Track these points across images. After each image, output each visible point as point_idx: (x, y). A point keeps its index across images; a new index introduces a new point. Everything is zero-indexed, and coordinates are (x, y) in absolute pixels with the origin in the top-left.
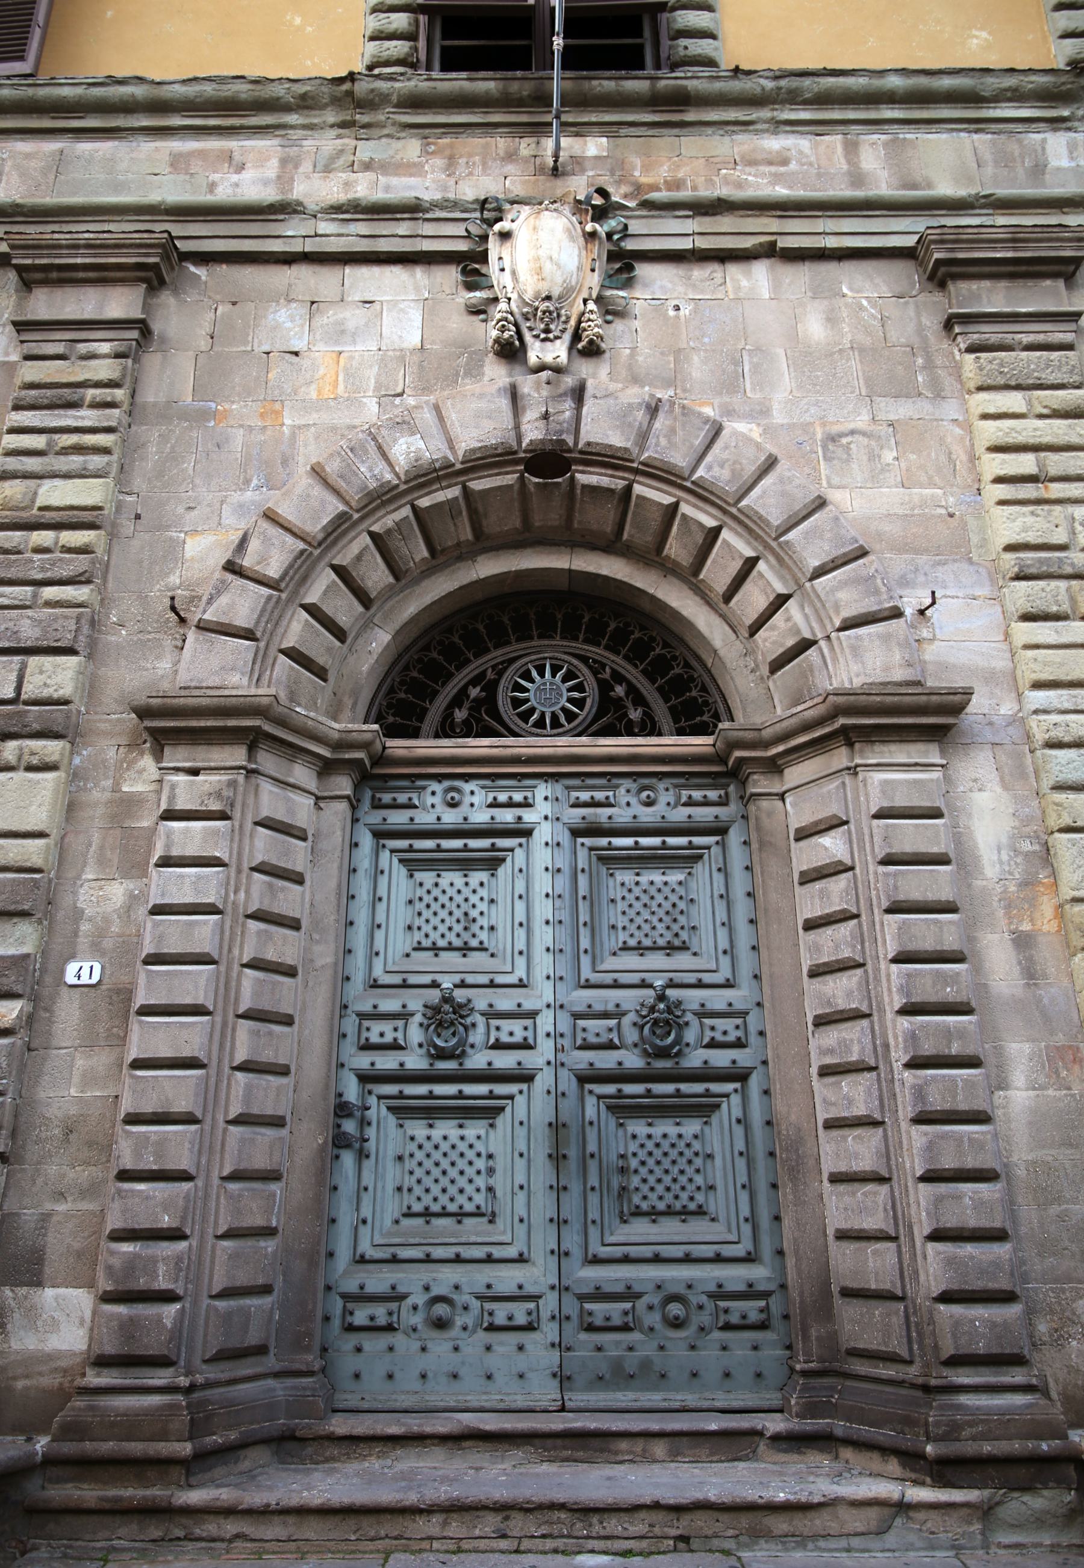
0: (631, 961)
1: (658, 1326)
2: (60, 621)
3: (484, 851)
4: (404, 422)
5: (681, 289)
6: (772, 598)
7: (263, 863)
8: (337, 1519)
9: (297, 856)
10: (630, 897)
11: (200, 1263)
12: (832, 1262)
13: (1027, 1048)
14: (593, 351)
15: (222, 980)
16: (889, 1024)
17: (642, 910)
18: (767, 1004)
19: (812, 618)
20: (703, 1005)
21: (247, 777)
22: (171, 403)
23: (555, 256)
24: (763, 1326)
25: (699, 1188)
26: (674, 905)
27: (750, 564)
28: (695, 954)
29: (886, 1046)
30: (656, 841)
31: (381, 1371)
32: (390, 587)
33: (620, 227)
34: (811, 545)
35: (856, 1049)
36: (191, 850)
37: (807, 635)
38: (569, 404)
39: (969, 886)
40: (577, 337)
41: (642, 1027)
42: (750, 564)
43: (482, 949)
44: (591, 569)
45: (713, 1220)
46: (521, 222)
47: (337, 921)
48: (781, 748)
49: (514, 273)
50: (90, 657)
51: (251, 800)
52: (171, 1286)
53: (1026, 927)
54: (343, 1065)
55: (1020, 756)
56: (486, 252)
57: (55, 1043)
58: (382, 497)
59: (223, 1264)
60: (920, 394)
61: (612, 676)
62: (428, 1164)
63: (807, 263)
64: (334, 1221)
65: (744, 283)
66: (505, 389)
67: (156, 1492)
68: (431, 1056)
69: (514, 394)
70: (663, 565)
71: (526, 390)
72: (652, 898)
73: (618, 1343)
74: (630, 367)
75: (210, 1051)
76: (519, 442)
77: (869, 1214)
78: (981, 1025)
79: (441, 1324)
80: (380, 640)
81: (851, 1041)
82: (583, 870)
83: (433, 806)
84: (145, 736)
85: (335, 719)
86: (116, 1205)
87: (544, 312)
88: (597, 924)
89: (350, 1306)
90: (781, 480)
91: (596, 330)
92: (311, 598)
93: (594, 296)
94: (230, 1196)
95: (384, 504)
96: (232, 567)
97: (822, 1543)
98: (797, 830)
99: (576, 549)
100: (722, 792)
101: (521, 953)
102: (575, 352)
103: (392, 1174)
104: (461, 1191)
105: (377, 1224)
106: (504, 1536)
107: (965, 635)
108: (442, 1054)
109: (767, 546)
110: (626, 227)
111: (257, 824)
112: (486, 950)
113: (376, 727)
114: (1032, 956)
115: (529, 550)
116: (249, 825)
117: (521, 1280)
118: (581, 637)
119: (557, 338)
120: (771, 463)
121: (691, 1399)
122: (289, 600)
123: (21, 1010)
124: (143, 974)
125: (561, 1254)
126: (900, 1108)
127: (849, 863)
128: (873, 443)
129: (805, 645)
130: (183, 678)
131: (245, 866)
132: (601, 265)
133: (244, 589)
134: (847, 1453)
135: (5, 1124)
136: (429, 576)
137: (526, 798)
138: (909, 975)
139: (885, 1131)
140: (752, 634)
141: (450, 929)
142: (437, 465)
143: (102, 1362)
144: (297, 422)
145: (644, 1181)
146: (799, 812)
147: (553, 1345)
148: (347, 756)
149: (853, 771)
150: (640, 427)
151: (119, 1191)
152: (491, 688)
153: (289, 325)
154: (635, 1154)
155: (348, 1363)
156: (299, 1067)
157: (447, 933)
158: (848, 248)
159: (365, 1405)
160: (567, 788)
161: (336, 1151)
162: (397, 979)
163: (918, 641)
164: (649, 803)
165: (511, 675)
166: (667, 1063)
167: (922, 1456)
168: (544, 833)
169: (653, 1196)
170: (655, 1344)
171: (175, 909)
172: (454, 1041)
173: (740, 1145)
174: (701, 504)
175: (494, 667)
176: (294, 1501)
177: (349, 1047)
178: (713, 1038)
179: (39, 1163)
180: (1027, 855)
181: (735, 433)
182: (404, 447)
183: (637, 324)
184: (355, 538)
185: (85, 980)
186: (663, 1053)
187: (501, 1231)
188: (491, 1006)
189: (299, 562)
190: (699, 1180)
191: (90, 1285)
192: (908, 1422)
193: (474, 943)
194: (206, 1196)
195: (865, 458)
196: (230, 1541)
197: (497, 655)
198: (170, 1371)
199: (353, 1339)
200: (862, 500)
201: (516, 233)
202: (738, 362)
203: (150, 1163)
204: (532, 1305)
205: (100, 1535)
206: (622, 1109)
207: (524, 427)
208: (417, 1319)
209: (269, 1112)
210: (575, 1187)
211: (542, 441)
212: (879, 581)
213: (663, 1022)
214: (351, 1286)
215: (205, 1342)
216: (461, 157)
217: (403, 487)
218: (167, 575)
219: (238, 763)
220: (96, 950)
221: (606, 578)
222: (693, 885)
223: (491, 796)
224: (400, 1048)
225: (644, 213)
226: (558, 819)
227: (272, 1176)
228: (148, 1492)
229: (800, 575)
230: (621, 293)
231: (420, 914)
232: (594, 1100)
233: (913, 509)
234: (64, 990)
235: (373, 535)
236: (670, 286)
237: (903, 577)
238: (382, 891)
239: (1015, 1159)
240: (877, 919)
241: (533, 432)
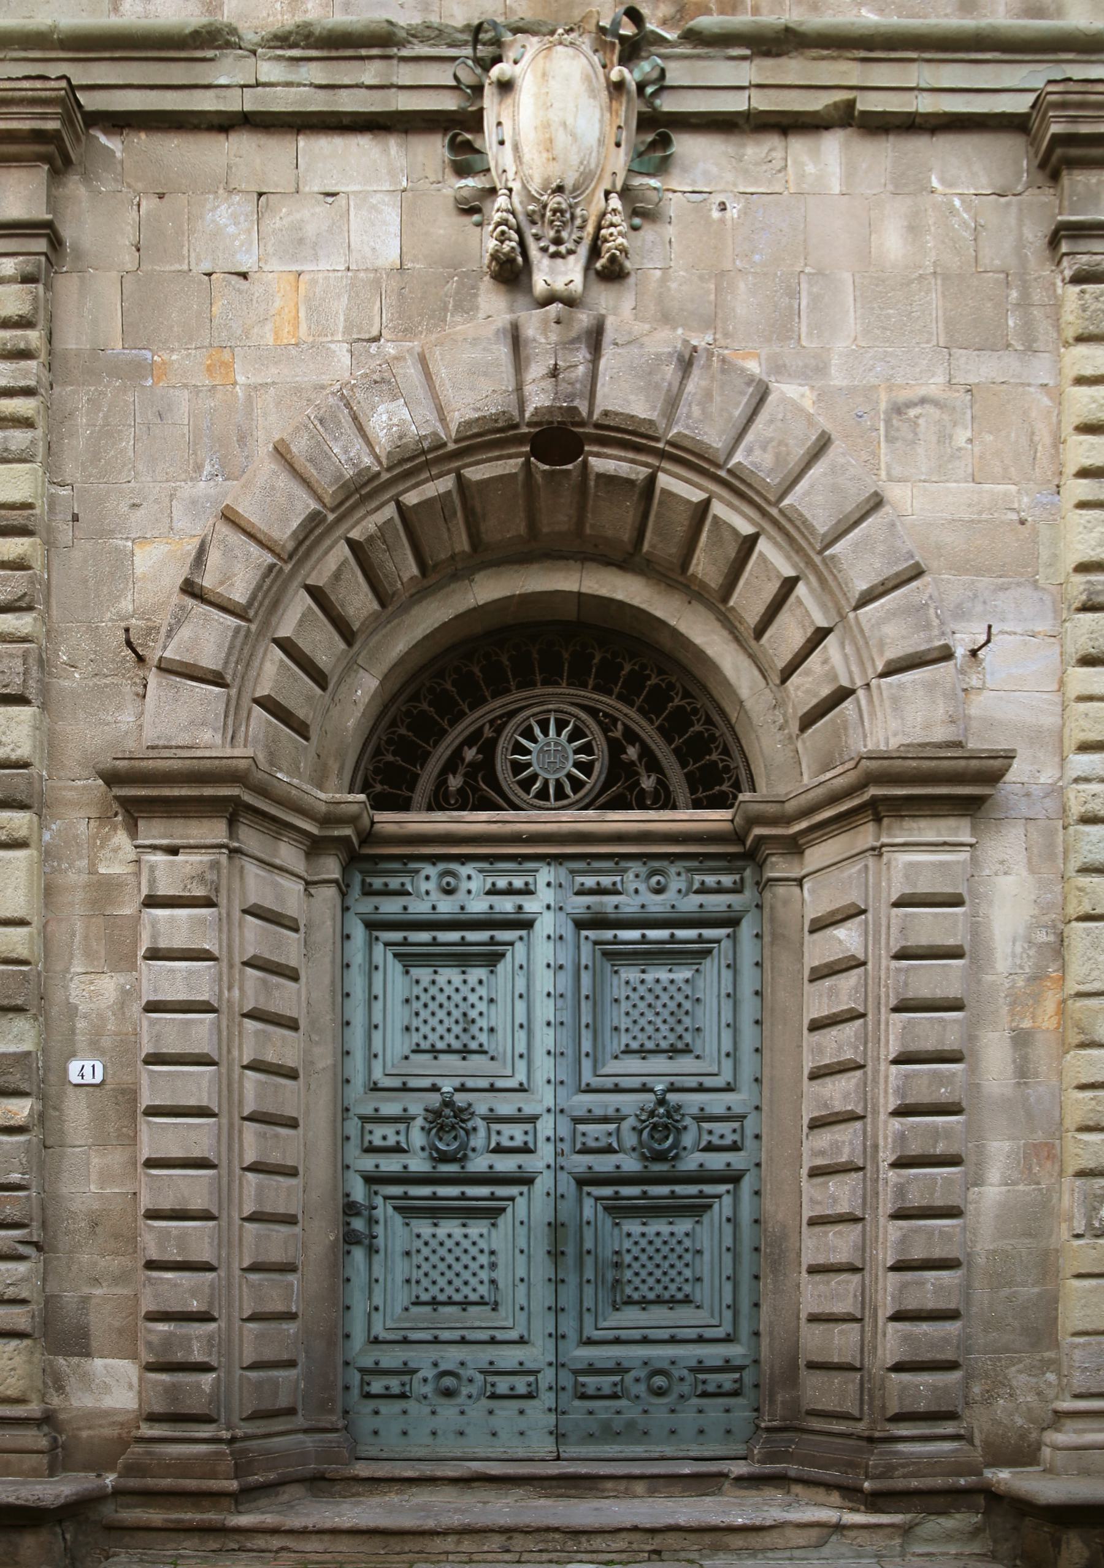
0: (633, 1064)
1: (643, 1395)
2: (6, 661)
3: (482, 943)
4: (383, 381)
5: (729, 176)
6: (810, 631)
7: (255, 957)
8: (364, 1538)
9: (289, 948)
10: (634, 996)
11: (229, 1341)
12: (801, 1341)
13: (1006, 1145)
15: (225, 1082)
16: (881, 1125)
17: (646, 1010)
18: (765, 1108)
19: (853, 660)
20: (702, 1109)
21: (230, 858)
22: (98, 351)
24: (735, 1394)
25: (687, 1280)
26: (679, 1005)
27: (789, 585)
28: (698, 1057)
29: (876, 1147)
30: (663, 934)
31: (396, 1427)
32: (375, 616)
33: (655, 74)
34: (860, 562)
35: (846, 1150)
36: (179, 941)
37: (845, 683)
38: (582, 354)
39: (979, 982)
40: (595, 252)
41: (641, 1132)
42: (789, 585)
43: (482, 1051)
44: (604, 592)
45: (698, 1307)
47: (333, 1020)
48: (804, 825)
49: (516, 148)
50: (43, 707)
51: (236, 885)
52: (206, 1359)
53: (1026, 1024)
54: (348, 1167)
55: (1050, 833)
57: (69, 1141)
58: (361, 491)
59: (251, 1342)
60: (1009, 345)
61: (624, 735)
62: (434, 1259)
63: (891, 138)
64: (348, 1308)
65: (810, 169)
67: (211, 1517)
68: (434, 1159)
69: (516, 338)
70: (687, 587)
72: (657, 997)
73: (607, 1408)
75: (219, 1152)
76: (522, 411)
77: (838, 1295)
78: (968, 1125)
79: (448, 1393)
80: (365, 688)
81: (843, 1142)
82: (586, 967)
83: (427, 893)
84: (116, 806)
85: (320, 787)
86: (148, 1290)
87: (554, 212)
88: (599, 1025)
89: (367, 1378)
90: (833, 470)
91: (620, 240)
92: (285, 631)
93: (619, 187)
94: (251, 1286)
95: (365, 499)
96: (191, 589)
97: (770, 1554)
98: (813, 921)
99: (588, 564)
100: (737, 877)
101: (521, 1056)
102: (592, 273)
103: (401, 1268)
104: (466, 1283)
105: (388, 1310)
106: (508, 1551)
107: (1013, 686)
108: (444, 1158)
109: (810, 563)
110: (663, 72)
111: (245, 911)
112: (486, 1052)
113: (362, 797)
114: (1027, 1054)
115: (535, 567)
116: (237, 914)
117: (522, 1359)
118: (591, 682)
119: (571, 252)
120: (823, 445)
121: (669, 1451)
122: (260, 633)
123: (31, 1109)
124: (146, 1073)
125: (558, 1337)
126: (881, 1205)
127: (862, 957)
128: (945, 417)
129: (842, 694)
130: (150, 735)
131: (237, 960)
133: (207, 619)
134: (797, 1489)
135: (35, 1216)
136: (420, 601)
137: (527, 884)
138: (907, 1076)
139: (864, 1227)
140: (784, 681)
141: (449, 1030)
142: (426, 445)
143: (153, 1418)
144: (252, 381)
145: (637, 1274)
146: (816, 901)
147: (550, 1410)
148: (336, 833)
149: (877, 851)
150: (669, 390)
151: (149, 1279)
152: (489, 749)
153: (232, 229)
154: (628, 1251)
155: (366, 1423)
156: (307, 1169)
157: (446, 1035)
158: (946, 114)
159: (385, 1455)
160: (572, 872)
161: (347, 1247)
162: (396, 1083)
163: (965, 690)
164: (659, 890)
165: (511, 733)
166: (662, 1166)
167: (860, 1490)
168: (546, 924)
169: (644, 1288)
170: (640, 1409)
171: (169, 1007)
172: (455, 1146)
173: (728, 1241)
174: (736, 502)
175: (492, 722)
176: (328, 1525)
177: (353, 1151)
178: (710, 1142)
179: (71, 1252)
180: (1040, 946)
181: (784, 399)
182: (384, 417)
183: (670, 231)
184: (331, 548)
185: (88, 1079)
186: (660, 1157)
187: (503, 1317)
188: (491, 1110)
189: (268, 581)
190: (688, 1273)
191: (134, 1357)
192: (852, 1465)
193: (473, 1045)
194: (229, 1285)
195: (934, 439)
196: (277, 1552)
197: (496, 706)
198: (213, 1427)
199: (372, 1404)
200: (927, 500)
201: (519, 82)
202: (794, 294)
203: (174, 1255)
204: (532, 1379)
205: (168, 1546)
206: (618, 1210)
207: (528, 389)
208: (427, 1389)
209: (282, 1210)
210: (572, 1279)
211: (550, 409)
212: (932, 611)
213: (662, 1126)
214: (368, 1362)
215: (241, 1404)
217: (386, 476)
218: (117, 599)
219: (218, 841)
220: (96, 1049)
221: (621, 604)
222: (700, 983)
223: (490, 880)
224: (404, 1151)
226: (561, 908)
227: (289, 1268)
228: (205, 1516)
229: (843, 602)
230: (653, 182)
231: (417, 1014)
232: (591, 1201)
233: (980, 513)
234: (70, 1090)
235: (352, 544)
236: (714, 170)
237: (959, 606)
238: (377, 989)
239: (978, 1248)
240: (883, 1018)
241: (539, 397)
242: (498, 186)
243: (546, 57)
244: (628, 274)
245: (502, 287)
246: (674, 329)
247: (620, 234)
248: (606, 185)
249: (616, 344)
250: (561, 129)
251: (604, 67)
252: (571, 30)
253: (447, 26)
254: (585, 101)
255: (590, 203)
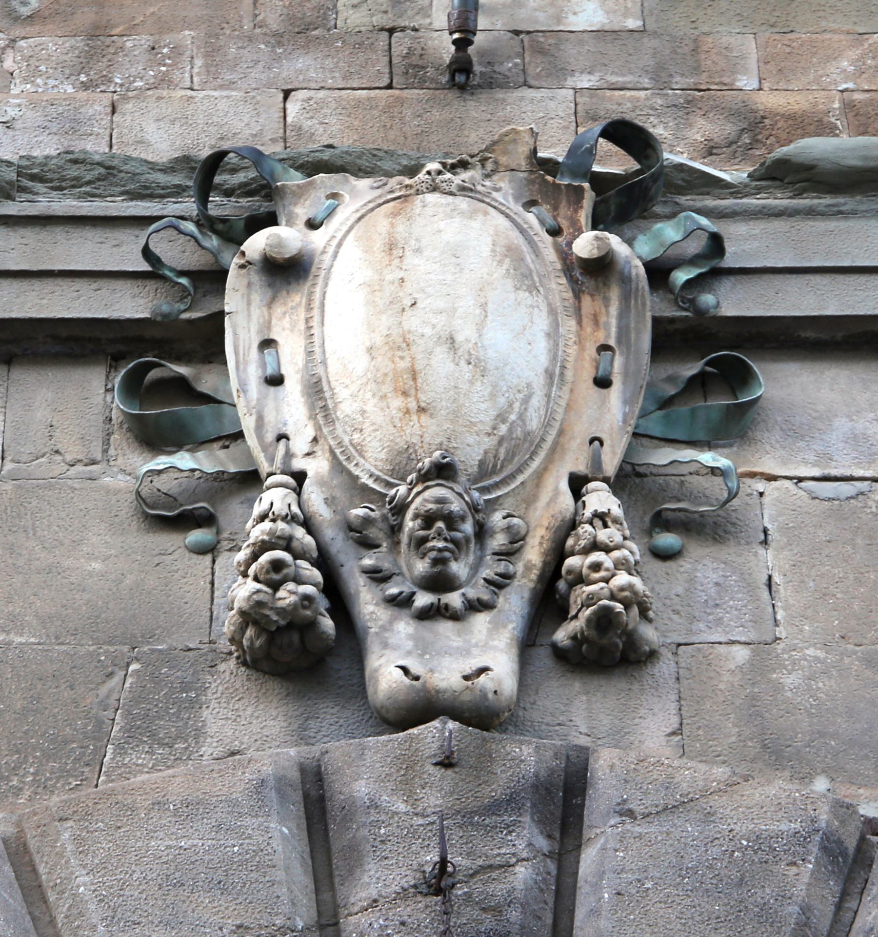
14: (611, 652)
23: (465, 333)
33: (695, 246)
38: (526, 838)
40: (549, 601)
46: (347, 237)
49: (316, 391)
56: (214, 325)
66: (281, 784)
69: (316, 804)
71: (362, 789)
74: (752, 710)
87: (428, 520)
91: (622, 578)
93: (611, 465)
102: (543, 657)
110: (716, 244)
119: (475, 606)
132: (632, 364)
183: (770, 560)
216: (132, 30)
225: (780, 201)
230: (708, 458)
242: (264, 468)
243: (395, 214)
244: (652, 655)
245: (274, 686)
246: (806, 779)
247: (620, 565)
248: (576, 460)
249: (630, 814)
250: (441, 354)
251: (555, 232)
252: (463, 165)
253: (128, 159)
254: (504, 291)
255: (530, 501)
